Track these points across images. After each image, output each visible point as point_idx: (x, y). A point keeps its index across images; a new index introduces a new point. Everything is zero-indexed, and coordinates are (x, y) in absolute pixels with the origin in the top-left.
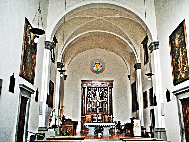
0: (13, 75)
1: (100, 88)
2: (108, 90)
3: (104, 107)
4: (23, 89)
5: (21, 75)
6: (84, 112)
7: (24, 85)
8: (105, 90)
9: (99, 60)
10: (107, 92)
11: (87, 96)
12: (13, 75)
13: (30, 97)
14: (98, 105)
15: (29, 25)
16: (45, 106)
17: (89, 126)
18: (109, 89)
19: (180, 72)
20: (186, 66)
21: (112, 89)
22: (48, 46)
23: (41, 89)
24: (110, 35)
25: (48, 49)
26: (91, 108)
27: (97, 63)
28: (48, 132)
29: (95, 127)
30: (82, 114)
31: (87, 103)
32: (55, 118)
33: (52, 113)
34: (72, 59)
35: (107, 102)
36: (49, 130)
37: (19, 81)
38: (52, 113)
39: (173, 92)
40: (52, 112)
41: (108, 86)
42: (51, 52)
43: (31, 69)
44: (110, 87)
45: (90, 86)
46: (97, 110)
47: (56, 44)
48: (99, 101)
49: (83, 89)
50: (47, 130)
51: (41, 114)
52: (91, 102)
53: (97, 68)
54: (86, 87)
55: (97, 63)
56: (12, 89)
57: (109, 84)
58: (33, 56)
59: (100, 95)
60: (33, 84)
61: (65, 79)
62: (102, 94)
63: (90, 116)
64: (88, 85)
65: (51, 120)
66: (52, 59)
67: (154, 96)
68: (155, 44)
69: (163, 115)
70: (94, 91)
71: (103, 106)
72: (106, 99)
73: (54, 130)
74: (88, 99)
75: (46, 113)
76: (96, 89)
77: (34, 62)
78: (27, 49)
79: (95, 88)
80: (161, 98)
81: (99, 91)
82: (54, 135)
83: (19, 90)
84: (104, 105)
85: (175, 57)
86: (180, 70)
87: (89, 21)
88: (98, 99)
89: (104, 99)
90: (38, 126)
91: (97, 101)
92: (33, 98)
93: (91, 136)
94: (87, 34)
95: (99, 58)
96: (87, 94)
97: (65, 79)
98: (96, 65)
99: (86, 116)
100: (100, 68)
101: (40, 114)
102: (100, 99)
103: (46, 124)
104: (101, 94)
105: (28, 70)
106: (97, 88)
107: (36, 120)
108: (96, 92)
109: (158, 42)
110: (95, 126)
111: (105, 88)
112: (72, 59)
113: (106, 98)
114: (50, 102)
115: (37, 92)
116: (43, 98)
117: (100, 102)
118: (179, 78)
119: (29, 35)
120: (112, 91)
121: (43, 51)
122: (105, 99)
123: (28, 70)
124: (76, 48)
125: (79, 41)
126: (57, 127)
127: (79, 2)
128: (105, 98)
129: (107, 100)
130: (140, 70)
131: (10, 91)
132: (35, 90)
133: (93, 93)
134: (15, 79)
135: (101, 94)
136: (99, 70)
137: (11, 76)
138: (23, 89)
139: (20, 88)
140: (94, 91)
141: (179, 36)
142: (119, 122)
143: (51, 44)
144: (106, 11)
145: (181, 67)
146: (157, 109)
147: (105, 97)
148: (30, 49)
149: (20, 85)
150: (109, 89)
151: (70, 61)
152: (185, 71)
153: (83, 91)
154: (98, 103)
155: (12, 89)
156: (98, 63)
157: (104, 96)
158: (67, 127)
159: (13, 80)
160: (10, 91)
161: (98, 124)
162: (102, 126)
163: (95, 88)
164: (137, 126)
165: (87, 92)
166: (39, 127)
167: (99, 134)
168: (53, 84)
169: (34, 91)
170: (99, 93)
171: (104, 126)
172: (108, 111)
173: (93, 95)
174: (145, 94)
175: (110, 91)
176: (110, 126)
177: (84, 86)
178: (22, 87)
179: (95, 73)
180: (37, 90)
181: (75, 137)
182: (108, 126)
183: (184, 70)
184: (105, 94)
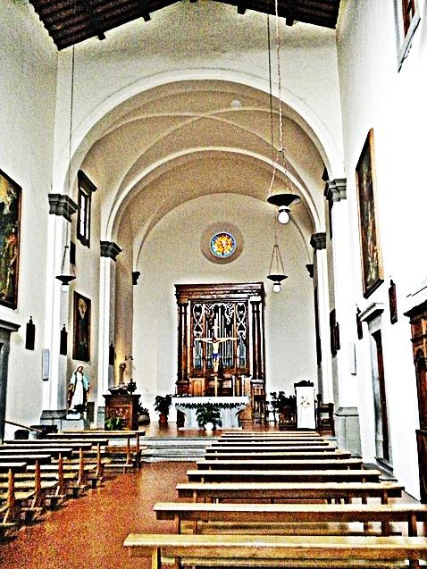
1: (225, 305)
2: (247, 309)
3: (238, 355)
6: (186, 370)
8: (240, 308)
9: (227, 225)
10: (247, 314)
13: (8, 339)
14: (216, 351)
17: (183, 405)
18: (250, 306)
22: (57, 206)
23: (42, 319)
24: (131, 197)
25: (57, 214)
26: (204, 358)
27: (220, 235)
28: (64, 422)
29: (199, 407)
30: (179, 374)
31: (192, 347)
32: (84, 389)
34: (150, 229)
36: (69, 417)
38: (74, 375)
40: (75, 374)
41: (249, 297)
43: (6, 274)
45: (200, 301)
47: (93, 193)
49: (181, 309)
50: (64, 418)
51: (47, 380)
53: (222, 247)
54: (189, 302)
55: (220, 235)
58: (8, 241)
61: (135, 283)
62: (232, 319)
64: (193, 297)
65: (71, 394)
68: (337, 185)
69: (355, 374)
70: (211, 314)
71: (235, 351)
72: (244, 333)
73: (82, 418)
76: (217, 307)
77: (13, 255)
79: (214, 305)
81: (223, 314)
82: (81, 428)
84: (238, 349)
87: (168, 131)
88: (216, 336)
90: (40, 405)
91: (214, 339)
92: (18, 342)
93: (190, 432)
94: (178, 158)
95: (224, 219)
97: (135, 283)
98: (219, 239)
99: (191, 380)
100: (229, 247)
101: (44, 380)
102: (228, 333)
103: (61, 402)
104: (229, 320)
106: (219, 305)
109: (345, 180)
110: (199, 405)
111: (241, 304)
112: (150, 229)
113: (244, 330)
115: (31, 329)
116: (48, 338)
121: (44, 227)
124: (169, 190)
125: (161, 178)
129: (247, 335)
130: (324, 251)
135: (229, 320)
136: (227, 253)
142: (281, 393)
143: (65, 201)
144: (210, 99)
147: (241, 328)
150: (250, 306)
151: (147, 233)
153: (180, 313)
154: (216, 346)
156: (225, 235)
157: (239, 325)
158: (118, 408)
161: (204, 400)
162: (216, 405)
163: (214, 305)
164: (305, 404)
165: (192, 316)
166: (45, 412)
167: (209, 426)
169: (17, 327)
171: (221, 404)
172: (248, 366)
175: (253, 312)
176: (238, 404)
177: (185, 301)
179: (218, 263)
182: (232, 406)
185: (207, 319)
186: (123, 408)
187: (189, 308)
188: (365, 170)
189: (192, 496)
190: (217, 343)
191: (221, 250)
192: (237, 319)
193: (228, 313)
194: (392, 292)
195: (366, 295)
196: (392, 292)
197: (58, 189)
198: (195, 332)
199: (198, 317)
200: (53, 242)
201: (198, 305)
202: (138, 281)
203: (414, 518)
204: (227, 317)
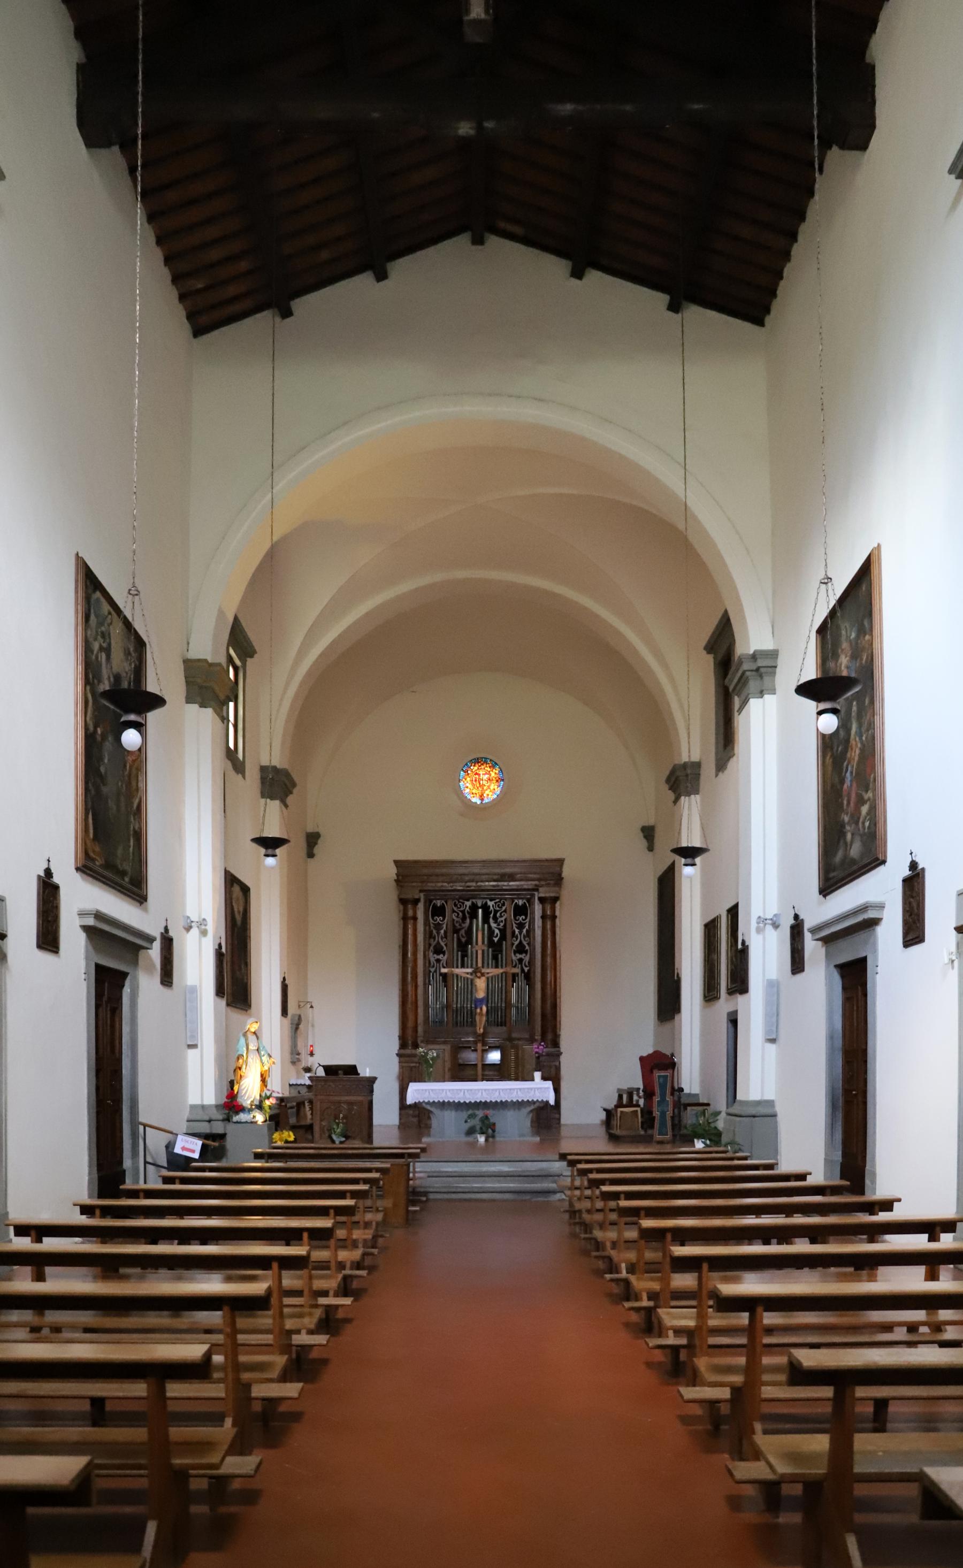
0: (48, 872)
1: (490, 904)
2: (533, 913)
3: (514, 1000)
4: (101, 933)
5: (86, 868)
7: (99, 916)
11: (427, 946)
12: (48, 872)
15: (98, 594)
16: (208, 1003)
18: (538, 908)
19: (848, 828)
20: (869, 799)
21: (558, 904)
33: (242, 1040)
35: (528, 977)
37: (82, 897)
38: (242, 1040)
39: (813, 931)
42: (225, 719)
44: (543, 892)
46: (478, 1018)
48: (483, 975)
52: (444, 976)
54: (422, 895)
55: (477, 761)
56: (48, 939)
57: (539, 880)
59: (496, 940)
60: (141, 903)
62: (503, 931)
63: (442, 1047)
64: (430, 886)
66: (231, 755)
67: (740, 946)
69: (773, 1041)
70: (464, 919)
71: (508, 993)
74: (432, 960)
75: (217, 1040)
76: (474, 908)
78: (95, 727)
79: (468, 904)
80: (766, 954)
81: (486, 920)
83: (82, 936)
85: (832, 749)
86: (846, 819)
88: (480, 965)
89: (515, 958)
96: (429, 936)
101: (191, 1046)
102: (495, 958)
104: (497, 931)
105: (113, 838)
107: (176, 1076)
108: (471, 924)
111: (521, 902)
113: (526, 952)
114: (234, 986)
115: (168, 943)
116: (198, 962)
117: (488, 978)
118: (840, 854)
119: (101, 649)
120: (554, 917)
122: (521, 960)
123: (113, 838)
126: (676, 1098)
127: (345, 423)
128: (519, 956)
131: (40, 946)
132: (155, 931)
133: (456, 931)
134: (56, 888)
137: (39, 877)
138: (101, 933)
139: (86, 928)
140: (464, 919)
141: (853, 635)
145: (852, 804)
146: (754, 1007)
147: (521, 949)
148: (116, 697)
149: (82, 914)
150: (538, 908)
152: (863, 823)
153: (405, 919)
154: (481, 984)
155: (48, 939)
159: (48, 891)
160: (40, 946)
163: (468, 904)
168: (245, 890)
169: (151, 940)
170: (490, 927)
173: (459, 940)
174: (710, 928)
175: (544, 917)
178: (91, 921)
180: (166, 929)
181: (334, 1146)
183: (861, 820)
184: (517, 931)
185: (456, 931)
186: (321, 1120)
187: (421, 906)
188: (848, 632)
189: (301, 1239)
190: (483, 979)
191: (478, 792)
192: (514, 932)
193: (495, 919)
194: (914, 884)
195: (828, 886)
196: (914, 884)
197: (196, 652)
198: (433, 957)
199: (438, 927)
200: (273, 748)
201: (439, 903)
202: (316, 850)
203: (705, 1266)
204: (493, 925)
